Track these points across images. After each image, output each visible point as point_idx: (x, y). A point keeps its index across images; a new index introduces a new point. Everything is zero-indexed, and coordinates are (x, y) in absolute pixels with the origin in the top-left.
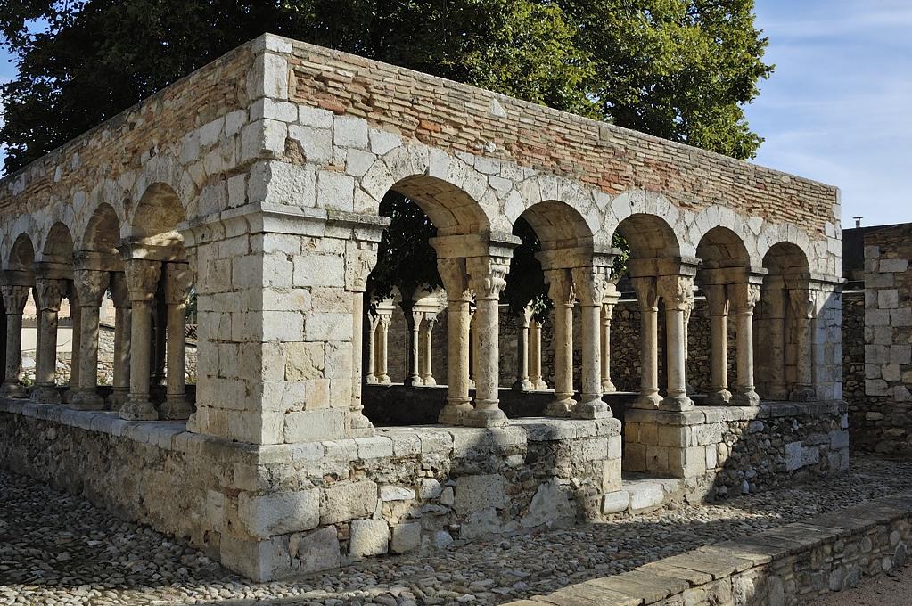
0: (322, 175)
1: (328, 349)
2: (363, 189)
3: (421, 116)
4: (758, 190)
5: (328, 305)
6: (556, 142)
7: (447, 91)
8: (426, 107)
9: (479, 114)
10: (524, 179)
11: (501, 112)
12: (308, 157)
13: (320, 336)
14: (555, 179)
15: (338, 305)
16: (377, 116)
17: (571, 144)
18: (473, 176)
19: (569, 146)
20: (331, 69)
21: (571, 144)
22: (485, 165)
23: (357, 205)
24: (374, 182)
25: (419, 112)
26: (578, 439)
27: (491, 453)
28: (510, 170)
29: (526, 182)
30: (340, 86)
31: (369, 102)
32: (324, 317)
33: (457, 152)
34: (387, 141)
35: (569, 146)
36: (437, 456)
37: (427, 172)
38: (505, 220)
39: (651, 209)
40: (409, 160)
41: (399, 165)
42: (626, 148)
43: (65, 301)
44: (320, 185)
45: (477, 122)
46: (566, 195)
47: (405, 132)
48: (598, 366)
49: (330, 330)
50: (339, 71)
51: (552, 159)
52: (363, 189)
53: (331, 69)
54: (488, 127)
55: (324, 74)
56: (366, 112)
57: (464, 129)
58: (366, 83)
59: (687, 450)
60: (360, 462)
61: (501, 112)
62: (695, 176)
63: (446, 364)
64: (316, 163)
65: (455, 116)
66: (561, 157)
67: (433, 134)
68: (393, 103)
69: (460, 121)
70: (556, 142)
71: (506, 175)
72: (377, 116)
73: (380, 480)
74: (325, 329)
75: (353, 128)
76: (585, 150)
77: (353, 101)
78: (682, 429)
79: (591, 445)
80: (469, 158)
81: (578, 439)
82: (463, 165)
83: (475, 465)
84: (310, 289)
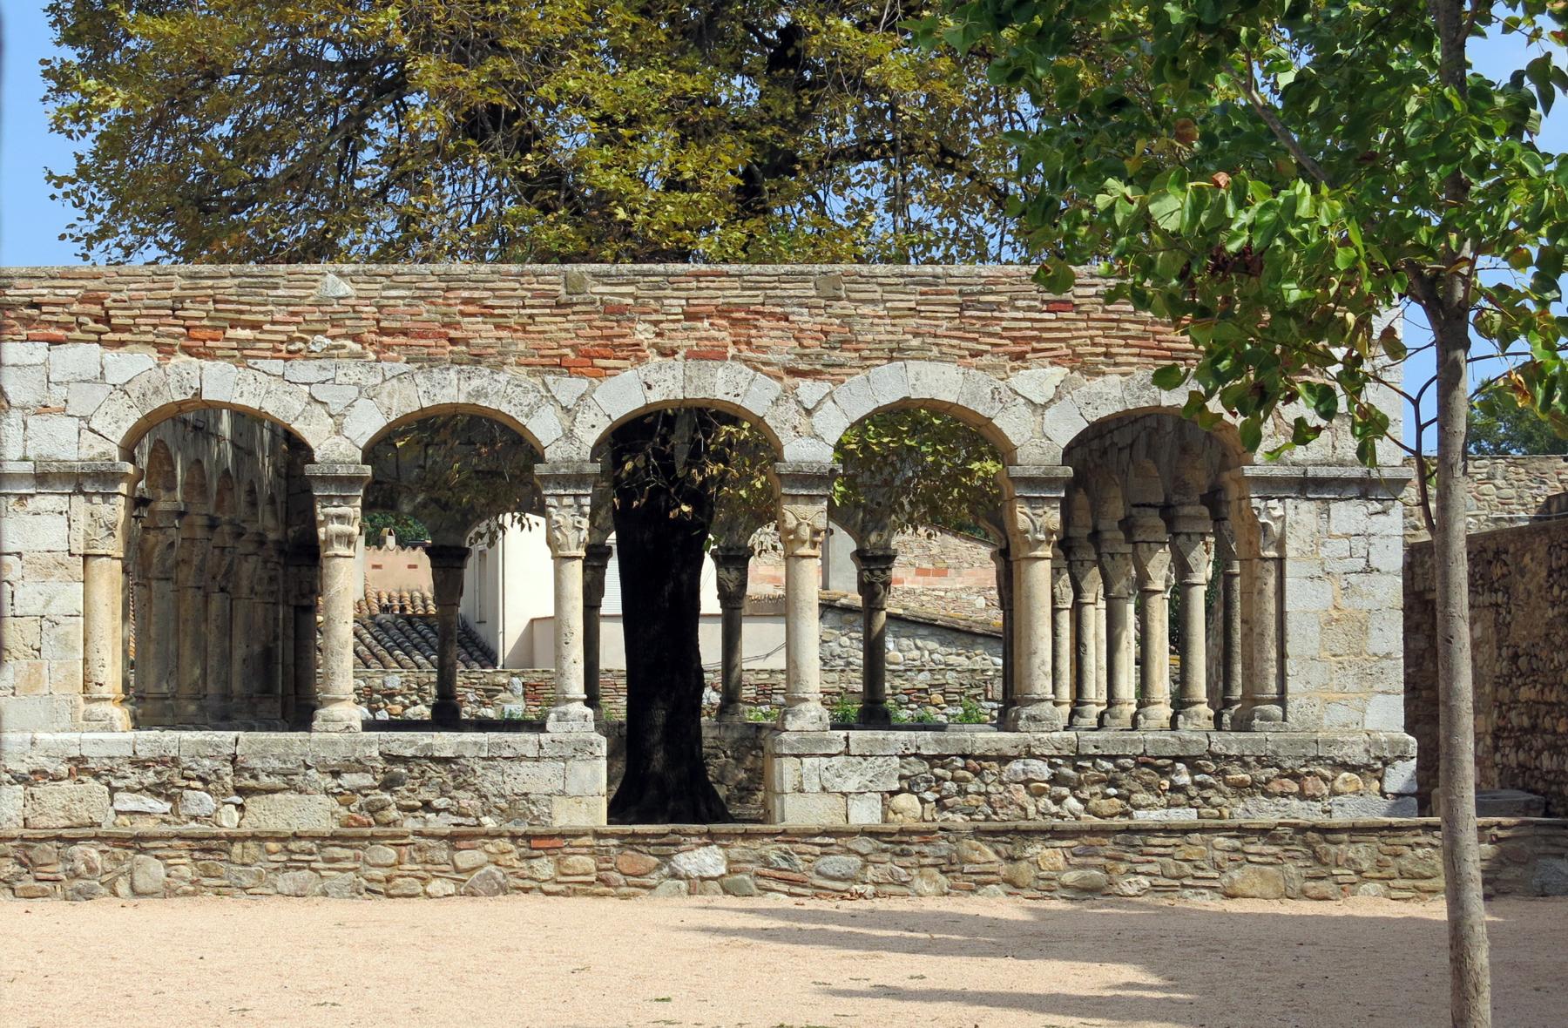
0: (31, 421)
1: (46, 625)
2: (92, 431)
3: (188, 323)
4: (1053, 316)
5: (45, 573)
6: (463, 314)
7: (237, 281)
8: (193, 311)
9: (293, 301)
10: (385, 380)
11: (345, 288)
12: (13, 402)
13: (32, 610)
14: (452, 372)
15: (58, 573)
16: (117, 336)
17: (497, 312)
18: (282, 389)
19: (492, 315)
20: (45, 291)
21: (497, 312)
22: (304, 370)
23: (83, 450)
24: (108, 419)
25: (184, 319)
26: (492, 759)
27: (308, 767)
28: (354, 371)
29: (388, 384)
30: (60, 309)
31: (106, 320)
32: (40, 587)
33: (251, 362)
34: (134, 363)
35: (492, 315)
36: (207, 762)
37: (198, 393)
38: (345, 443)
39: (697, 388)
40: (166, 384)
41: (149, 394)
42: (636, 298)
43: (1119, 222)
44: (30, 433)
45: (293, 314)
46: (479, 393)
47: (165, 351)
48: (1045, 630)
49: (48, 603)
50: (58, 291)
51: (453, 341)
52: (92, 431)
53: (45, 291)
54: (317, 316)
55: (36, 300)
56: (100, 333)
57: (267, 327)
58: (99, 298)
59: (788, 798)
60: (82, 759)
61: (345, 288)
62: (837, 317)
63: (1011, 599)
64: (23, 408)
65: (250, 312)
66: (471, 334)
67: (209, 343)
68: (141, 316)
69: (261, 317)
70: (463, 314)
71: (345, 379)
72: (117, 336)
73: (115, 783)
74: (41, 601)
75: (81, 357)
76: (531, 316)
77: (80, 325)
78: (776, 760)
79: (522, 771)
80: (277, 366)
81: (492, 759)
82: (261, 377)
83: (276, 781)
84: (19, 555)
